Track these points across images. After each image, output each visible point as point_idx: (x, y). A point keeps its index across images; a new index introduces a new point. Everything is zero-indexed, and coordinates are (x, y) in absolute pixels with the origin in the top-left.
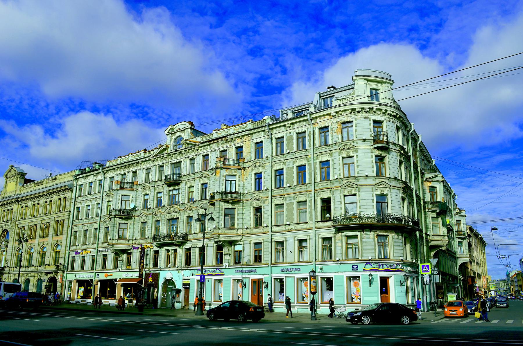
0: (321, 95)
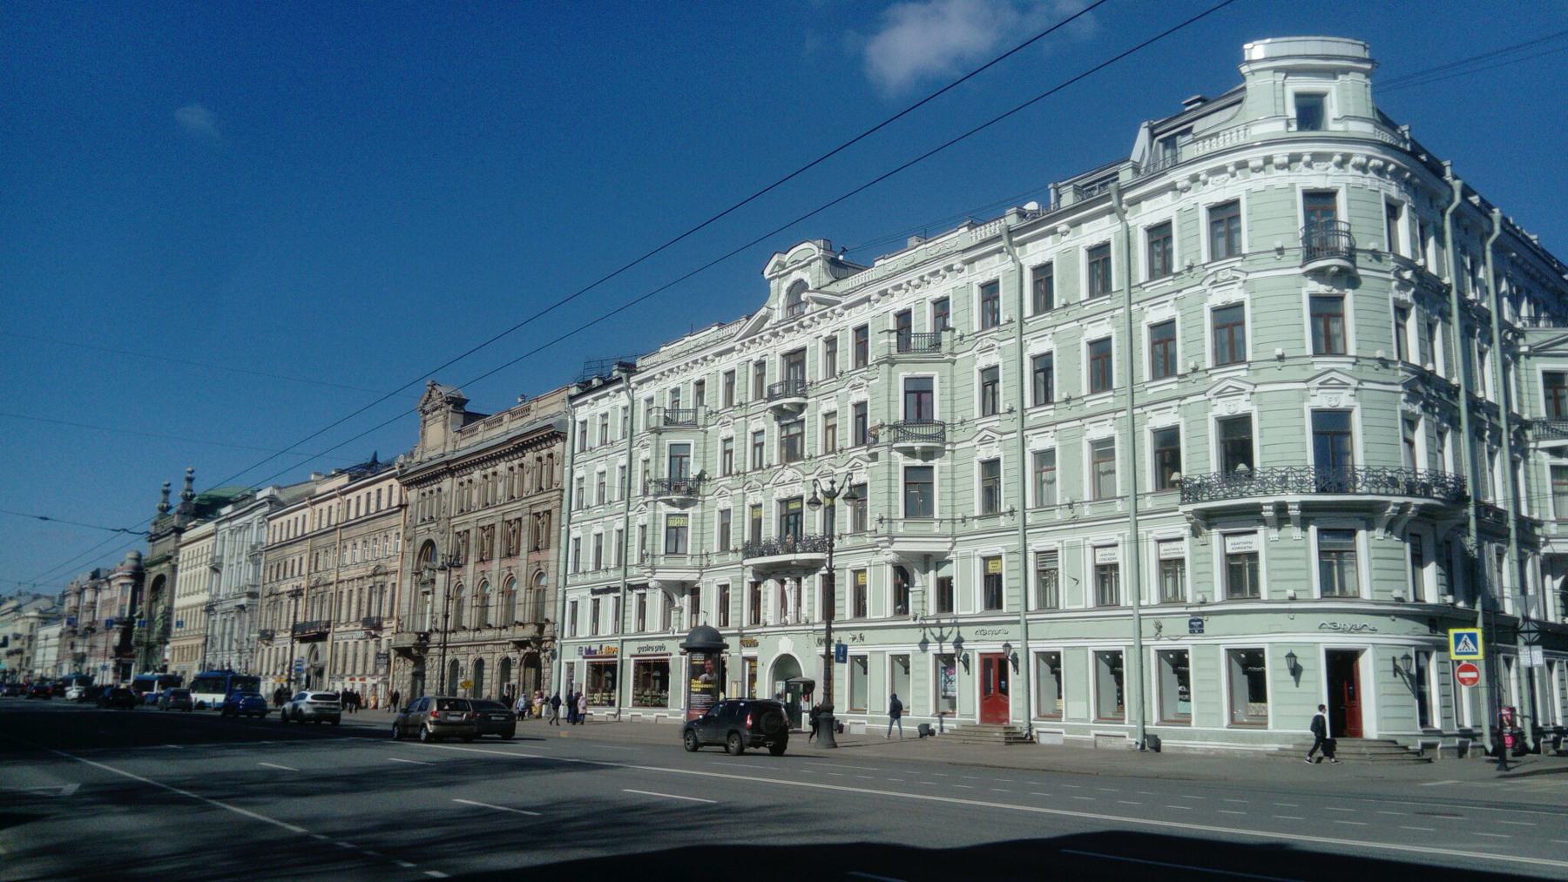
0: (1156, 131)
